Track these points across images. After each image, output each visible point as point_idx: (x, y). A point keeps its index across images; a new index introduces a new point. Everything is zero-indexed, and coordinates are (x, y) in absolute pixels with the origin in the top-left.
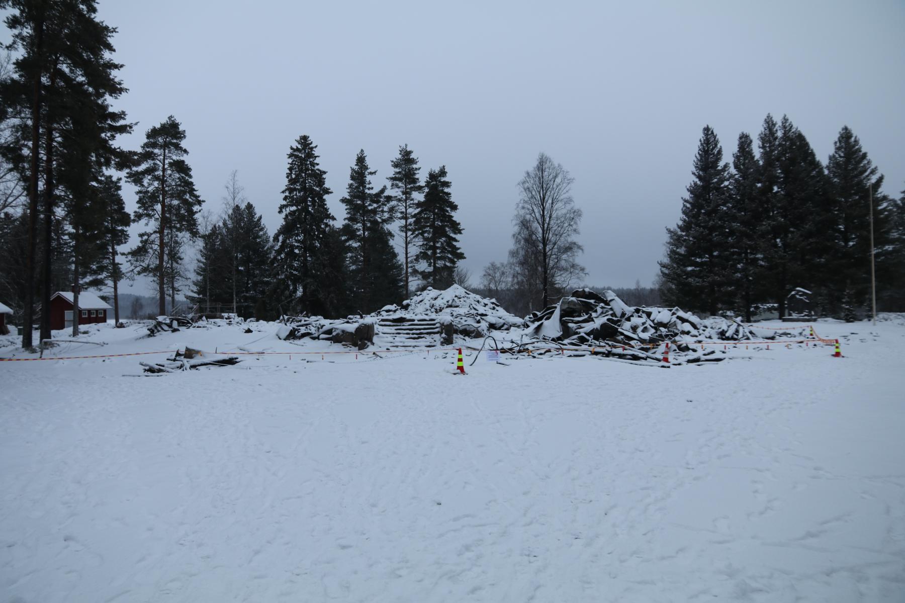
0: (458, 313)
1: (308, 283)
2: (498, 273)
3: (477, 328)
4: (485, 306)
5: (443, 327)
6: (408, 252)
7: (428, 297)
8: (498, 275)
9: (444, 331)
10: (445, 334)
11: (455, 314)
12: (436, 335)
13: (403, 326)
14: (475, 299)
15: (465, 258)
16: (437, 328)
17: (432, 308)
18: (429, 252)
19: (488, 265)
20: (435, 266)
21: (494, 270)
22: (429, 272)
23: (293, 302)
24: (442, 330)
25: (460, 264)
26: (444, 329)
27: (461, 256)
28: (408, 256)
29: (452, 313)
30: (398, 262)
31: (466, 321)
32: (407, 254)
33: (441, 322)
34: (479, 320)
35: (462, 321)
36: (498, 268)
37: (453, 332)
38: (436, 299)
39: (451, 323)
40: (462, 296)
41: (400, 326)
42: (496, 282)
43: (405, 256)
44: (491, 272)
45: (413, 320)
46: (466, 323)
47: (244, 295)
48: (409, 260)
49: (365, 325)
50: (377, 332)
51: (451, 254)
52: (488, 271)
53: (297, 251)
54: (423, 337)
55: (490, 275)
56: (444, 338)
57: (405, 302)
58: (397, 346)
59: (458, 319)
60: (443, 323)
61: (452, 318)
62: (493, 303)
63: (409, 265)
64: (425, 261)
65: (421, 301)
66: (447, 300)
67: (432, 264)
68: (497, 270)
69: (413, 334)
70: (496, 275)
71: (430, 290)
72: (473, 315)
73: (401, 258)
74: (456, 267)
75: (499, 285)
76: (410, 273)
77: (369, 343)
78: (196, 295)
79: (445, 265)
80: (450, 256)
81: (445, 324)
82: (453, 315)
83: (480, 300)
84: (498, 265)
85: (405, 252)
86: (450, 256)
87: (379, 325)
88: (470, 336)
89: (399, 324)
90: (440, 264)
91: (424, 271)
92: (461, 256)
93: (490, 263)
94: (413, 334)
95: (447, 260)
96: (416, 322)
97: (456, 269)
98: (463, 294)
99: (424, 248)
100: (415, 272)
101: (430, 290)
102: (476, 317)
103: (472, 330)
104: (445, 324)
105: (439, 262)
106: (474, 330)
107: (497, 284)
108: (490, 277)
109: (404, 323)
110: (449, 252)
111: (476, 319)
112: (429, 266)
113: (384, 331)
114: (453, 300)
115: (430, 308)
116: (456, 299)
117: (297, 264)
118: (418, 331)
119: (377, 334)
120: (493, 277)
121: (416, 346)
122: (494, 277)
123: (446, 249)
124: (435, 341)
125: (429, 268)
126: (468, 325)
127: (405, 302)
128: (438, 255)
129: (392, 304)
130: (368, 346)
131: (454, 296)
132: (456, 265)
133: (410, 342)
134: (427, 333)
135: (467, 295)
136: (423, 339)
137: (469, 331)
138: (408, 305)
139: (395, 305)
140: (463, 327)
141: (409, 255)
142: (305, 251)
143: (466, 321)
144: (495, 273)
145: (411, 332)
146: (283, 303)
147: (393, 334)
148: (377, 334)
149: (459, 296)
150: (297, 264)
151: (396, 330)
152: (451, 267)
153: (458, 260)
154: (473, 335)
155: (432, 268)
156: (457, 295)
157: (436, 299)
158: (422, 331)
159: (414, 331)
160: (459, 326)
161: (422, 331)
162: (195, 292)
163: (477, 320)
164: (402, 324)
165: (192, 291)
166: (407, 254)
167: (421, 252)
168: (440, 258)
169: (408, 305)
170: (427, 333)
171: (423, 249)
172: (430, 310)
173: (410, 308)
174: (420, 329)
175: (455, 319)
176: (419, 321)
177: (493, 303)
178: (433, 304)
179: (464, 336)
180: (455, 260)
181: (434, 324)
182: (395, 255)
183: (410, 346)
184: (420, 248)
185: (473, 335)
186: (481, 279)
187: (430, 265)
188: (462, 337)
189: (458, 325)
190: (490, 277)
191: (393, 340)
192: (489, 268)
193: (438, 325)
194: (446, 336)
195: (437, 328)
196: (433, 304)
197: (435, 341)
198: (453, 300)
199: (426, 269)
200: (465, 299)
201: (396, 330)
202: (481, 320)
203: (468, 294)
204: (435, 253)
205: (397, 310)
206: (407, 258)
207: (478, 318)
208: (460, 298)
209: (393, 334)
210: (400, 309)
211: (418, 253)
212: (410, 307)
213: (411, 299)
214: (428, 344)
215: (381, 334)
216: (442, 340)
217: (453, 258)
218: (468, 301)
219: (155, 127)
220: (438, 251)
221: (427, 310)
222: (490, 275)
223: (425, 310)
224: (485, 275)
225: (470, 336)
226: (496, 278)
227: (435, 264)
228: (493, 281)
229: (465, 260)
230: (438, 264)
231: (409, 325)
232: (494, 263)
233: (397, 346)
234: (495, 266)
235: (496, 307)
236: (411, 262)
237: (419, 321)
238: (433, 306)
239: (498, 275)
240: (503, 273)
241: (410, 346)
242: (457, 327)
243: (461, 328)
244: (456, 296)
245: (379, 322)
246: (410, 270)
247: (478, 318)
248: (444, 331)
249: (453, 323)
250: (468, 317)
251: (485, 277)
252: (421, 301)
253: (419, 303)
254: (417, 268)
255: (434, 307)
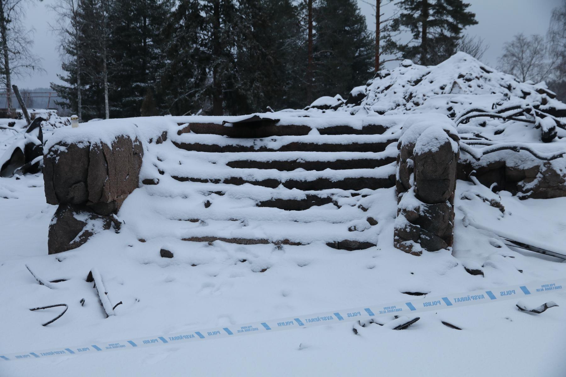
0: (469, 108)
1: (219, 64)
2: (528, 51)
3: (548, 161)
4: (524, 98)
5: (410, 161)
6: (380, 14)
7: (403, 80)
8: (527, 54)
9: (411, 180)
10: (418, 196)
11: (459, 110)
12: (381, 191)
13: (264, 149)
14: (503, 83)
15: (476, 23)
16: (387, 161)
17: (408, 101)
18: (417, 14)
19: (512, 39)
20: (424, 37)
21: (521, 47)
22: (414, 48)
23: (197, 95)
24: (405, 171)
25: (468, 32)
26: (411, 170)
27: (469, 20)
28: (381, 20)
29: (450, 109)
30: (368, 37)
31: (498, 133)
32: (378, 16)
33: (404, 140)
34: (552, 129)
35: (487, 132)
36: (528, 45)
37: (452, 172)
38: (417, 82)
39: (448, 144)
40: (474, 75)
41: (251, 149)
42: (523, 66)
43: (375, 21)
44: (516, 50)
45: (304, 130)
46: (499, 141)
47: (138, 85)
48: (381, 26)
49: (72, 147)
50: (155, 175)
51: (452, 17)
52: (511, 48)
53: (203, 14)
54: (328, 200)
55: (513, 55)
56: (410, 215)
57: (355, 91)
58: (210, 240)
59: (473, 126)
60: (412, 145)
61: (452, 126)
62: (541, 91)
63: (382, 34)
64: (409, 29)
65: (387, 88)
66: (441, 85)
67: (421, 34)
68: (526, 47)
69: (290, 184)
70: (524, 56)
71: (406, 66)
72: (528, 111)
73: (371, 26)
74: (459, 38)
75: (528, 70)
76: (383, 47)
77: (96, 225)
78: (67, 85)
79: (442, 34)
80: (450, 19)
81: (418, 149)
82: (453, 115)
83: (514, 84)
84: (529, 39)
85: (375, 14)
86: (450, 19)
87: (175, 144)
88: (520, 189)
89: (247, 143)
90: (433, 32)
91: (407, 46)
92: (469, 20)
93: (516, 36)
94: (290, 184)
95: (446, 25)
96: (314, 137)
97: (460, 41)
98: (477, 72)
99: (407, 7)
100: (391, 46)
101: (406, 66)
102: (538, 119)
103: (528, 166)
104: (418, 149)
105: (432, 30)
106: (536, 169)
107: (525, 69)
108: (515, 59)
109: (268, 142)
110: (449, 13)
111: (539, 126)
112: (414, 38)
113: (183, 172)
114: (455, 83)
115: (405, 102)
116: (460, 81)
117: (204, 34)
118: (312, 175)
119: (149, 182)
120: (518, 58)
121: (286, 242)
122: (520, 59)
123: (445, 8)
124: (372, 222)
125: (414, 40)
126: (514, 149)
127: (355, 91)
128: (431, 18)
129: (333, 96)
130: (88, 235)
131: (457, 76)
132: (461, 35)
133: (268, 220)
134: (345, 184)
135: (485, 74)
136: (327, 210)
137: (515, 169)
138: (361, 96)
139: (338, 96)
140: (494, 157)
141: (381, 19)
142: (217, 14)
143: (498, 133)
144: (523, 52)
145: (285, 175)
146: (183, 96)
147: (217, 181)
148: (149, 182)
149: (468, 77)
150: (204, 34)
151: (233, 164)
152: (452, 38)
153: (464, 26)
154: (530, 185)
155: (420, 40)
156: (464, 73)
157: (417, 82)
158: (328, 173)
159: (299, 174)
160: (478, 151)
161: (328, 173)
162: (66, 80)
163: (546, 129)
164: (259, 143)
165: (62, 78)
166: (378, 16)
167: (403, 15)
168: (433, 24)
169: (361, 96)
170: (345, 184)
171: (406, 9)
172: (404, 105)
173: (365, 101)
174: (319, 166)
175: (462, 126)
176: (323, 131)
177: (541, 91)
178: (411, 94)
179: (495, 190)
180: (460, 26)
181: (380, 147)
182: (361, 20)
183: (264, 242)
184: (401, 7)
185: (530, 185)
186: (500, 61)
187: (416, 37)
188: (487, 192)
189: (470, 148)
190: (515, 59)
191: (199, 210)
192: (513, 45)
193: (392, 150)
194: (422, 206)
195: (387, 161)
196: (411, 94)
197: (372, 222)
198: (455, 83)
199: (410, 42)
200: (481, 82)
201: (233, 164)
202: (558, 130)
203: (488, 72)
204: (425, 14)
205: (340, 105)
206: (378, 24)
207: (548, 122)
208: (469, 80)
209: (217, 181)
210: (346, 104)
211: (397, 16)
212: (365, 98)
213: (369, 85)
214: (342, 234)
215: (166, 182)
216: (402, 221)
217: (455, 23)
218: (487, 86)
219: (504, 162)
220: (431, 12)
221: (399, 105)
222: (513, 55)
223: (393, 105)
224: (505, 56)
225: (520, 189)
226: (524, 60)
227: (424, 33)
228: (519, 65)
229: (475, 25)
230: (430, 33)
231: (285, 148)
232: (521, 35)
233: (210, 240)
234: (523, 40)
235: (548, 98)
236: (385, 29)
237: (323, 131)
238: (411, 96)
239: (527, 54)
240: (536, 52)
241: (264, 242)
242: (469, 157)
243: (485, 161)
244: (461, 76)
245: (179, 133)
246: (382, 43)
247: (548, 122)
248: (411, 180)
249: (455, 146)
250: (510, 118)
251: (506, 59)
252: (387, 88)
253: (382, 92)
254: (393, 39)
255: (413, 99)
